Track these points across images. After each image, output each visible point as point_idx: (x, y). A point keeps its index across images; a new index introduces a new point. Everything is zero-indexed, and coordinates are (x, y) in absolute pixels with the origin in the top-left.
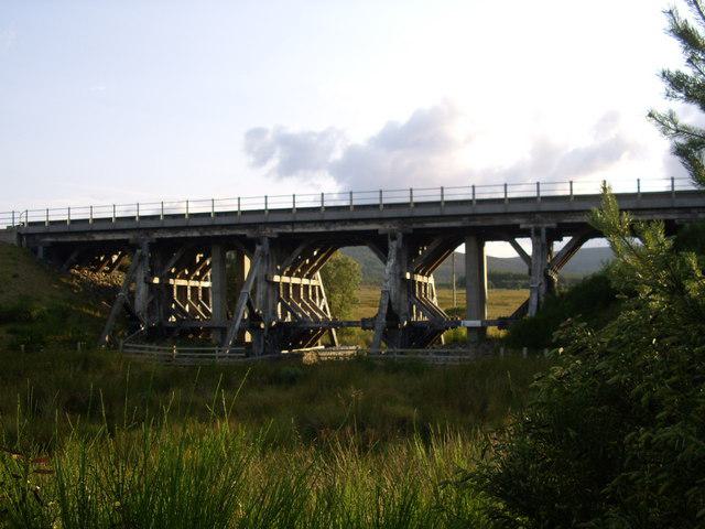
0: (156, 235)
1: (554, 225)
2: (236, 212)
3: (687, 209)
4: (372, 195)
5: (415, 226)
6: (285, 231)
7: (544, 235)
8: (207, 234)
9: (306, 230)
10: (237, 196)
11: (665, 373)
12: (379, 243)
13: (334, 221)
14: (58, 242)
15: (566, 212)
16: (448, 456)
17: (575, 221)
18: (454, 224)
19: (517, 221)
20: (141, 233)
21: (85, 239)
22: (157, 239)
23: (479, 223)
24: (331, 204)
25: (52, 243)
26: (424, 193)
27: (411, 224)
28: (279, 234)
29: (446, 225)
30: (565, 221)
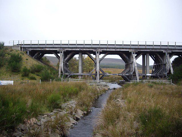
0: (66, 49)
1: (171, 52)
2: (115, 45)
3: (96, 48)
4: (17, 42)
5: (139, 50)
6: (104, 50)
7: (99, 53)
8: (81, 50)
9: (110, 50)
10: (122, 41)
11: (22, 84)
12: (56, 52)
13: (118, 48)
14: (34, 50)
15: (174, 49)
16: (33, 120)
17: (176, 51)
18: (148, 51)
19: (162, 51)
20: (61, 48)
21: (43, 50)
22: (66, 50)
23: (154, 51)
24: (170, 45)
25: (32, 50)
26: (34, 42)
27: (137, 50)
28: (102, 51)
29: (146, 50)
30: (173, 51)
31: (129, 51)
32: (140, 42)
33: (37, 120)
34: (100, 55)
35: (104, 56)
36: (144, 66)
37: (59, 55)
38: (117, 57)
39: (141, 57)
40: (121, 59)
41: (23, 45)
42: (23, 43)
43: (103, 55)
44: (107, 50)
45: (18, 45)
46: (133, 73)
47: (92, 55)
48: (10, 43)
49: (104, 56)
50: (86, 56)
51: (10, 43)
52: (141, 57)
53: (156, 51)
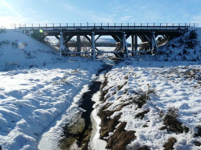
26: (118, 24)
31: (120, 32)
32: (175, 24)
33: (179, 128)
34: (95, 35)
35: (99, 37)
36: (135, 45)
37: (59, 36)
38: (110, 37)
39: (130, 38)
40: (113, 38)
41: (24, 27)
42: (24, 26)
43: (98, 36)
44: (101, 31)
45: (19, 28)
46: (124, 51)
47: (88, 36)
48: (12, 26)
49: (99, 37)
50: (82, 37)
51: (12, 26)
52: (130, 38)
53: (71, 32)
